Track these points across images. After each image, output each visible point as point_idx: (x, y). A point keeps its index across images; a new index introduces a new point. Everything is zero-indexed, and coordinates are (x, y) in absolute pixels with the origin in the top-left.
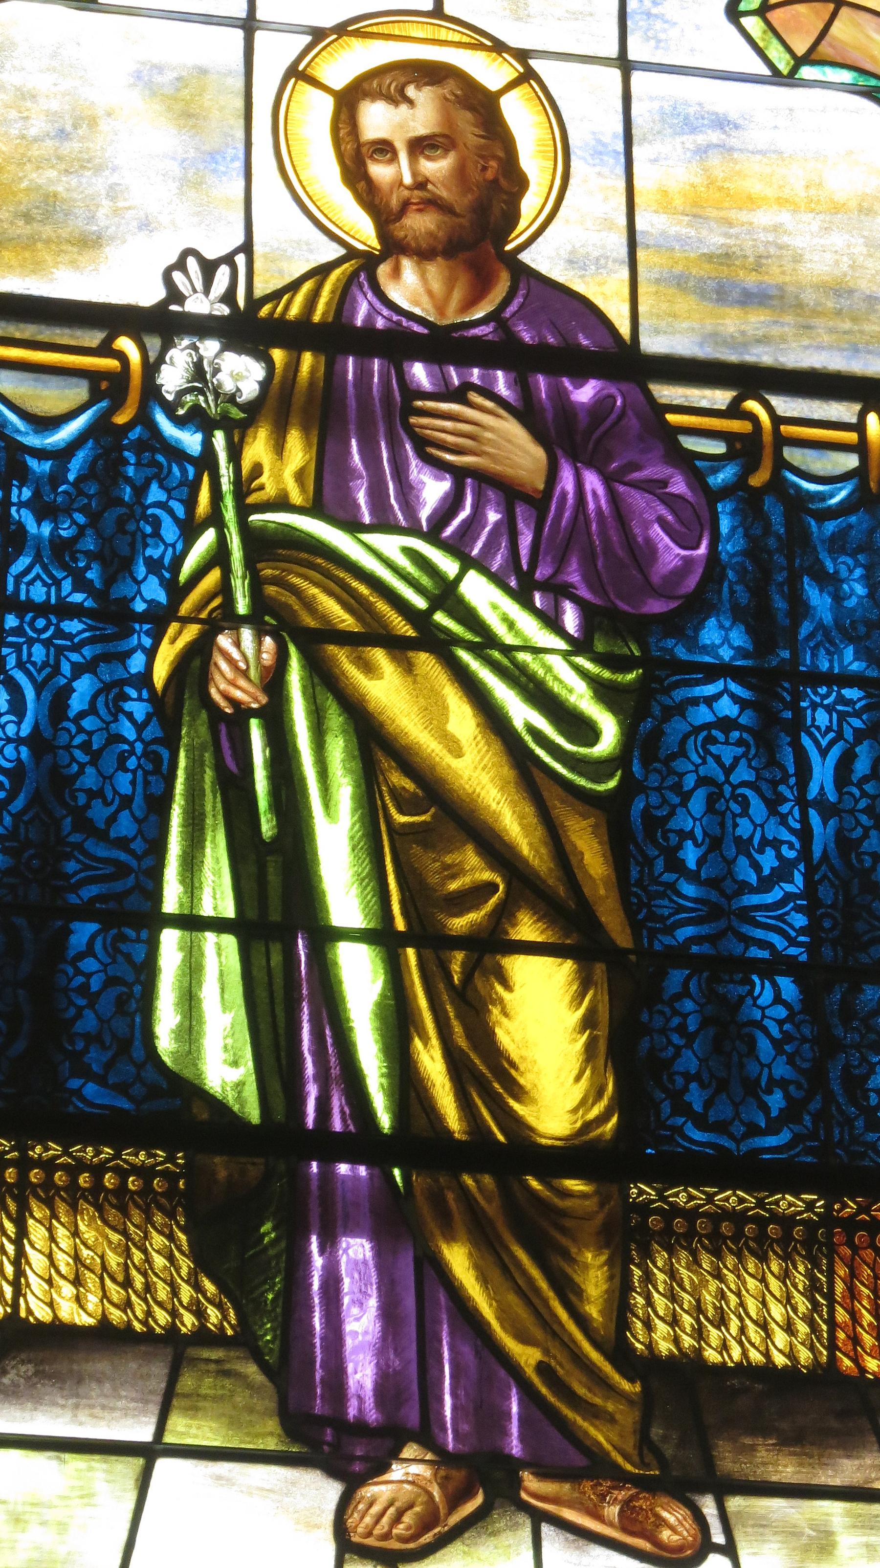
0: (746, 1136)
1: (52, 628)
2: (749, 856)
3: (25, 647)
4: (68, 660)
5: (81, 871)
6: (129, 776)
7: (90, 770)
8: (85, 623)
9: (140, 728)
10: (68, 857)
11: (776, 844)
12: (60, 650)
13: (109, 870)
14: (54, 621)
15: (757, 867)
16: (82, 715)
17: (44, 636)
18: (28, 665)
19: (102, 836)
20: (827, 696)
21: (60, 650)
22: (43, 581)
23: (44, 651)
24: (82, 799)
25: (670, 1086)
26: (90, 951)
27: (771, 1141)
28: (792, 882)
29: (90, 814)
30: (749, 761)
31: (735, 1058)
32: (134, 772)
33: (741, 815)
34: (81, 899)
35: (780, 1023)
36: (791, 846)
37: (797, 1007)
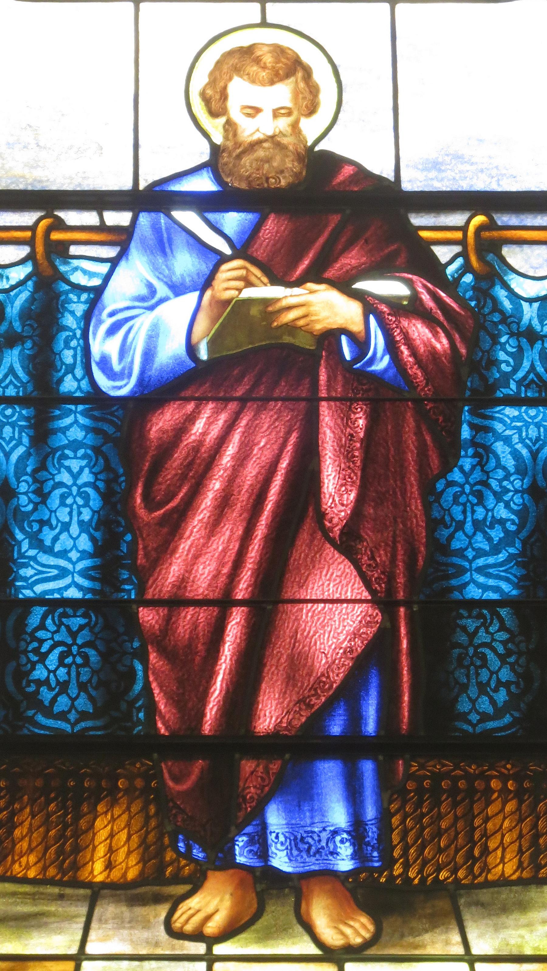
1: (17, 414)
2: (485, 533)
5: (36, 574)
6: (68, 510)
9: (75, 476)
13: (55, 572)
14: (18, 410)
15: (489, 539)
18: (527, 441)
20: (12, 415)
26: (42, 626)
28: (514, 546)
30: (91, 468)
31: (472, 669)
33: (477, 504)
35: (504, 643)
37: (512, 470)
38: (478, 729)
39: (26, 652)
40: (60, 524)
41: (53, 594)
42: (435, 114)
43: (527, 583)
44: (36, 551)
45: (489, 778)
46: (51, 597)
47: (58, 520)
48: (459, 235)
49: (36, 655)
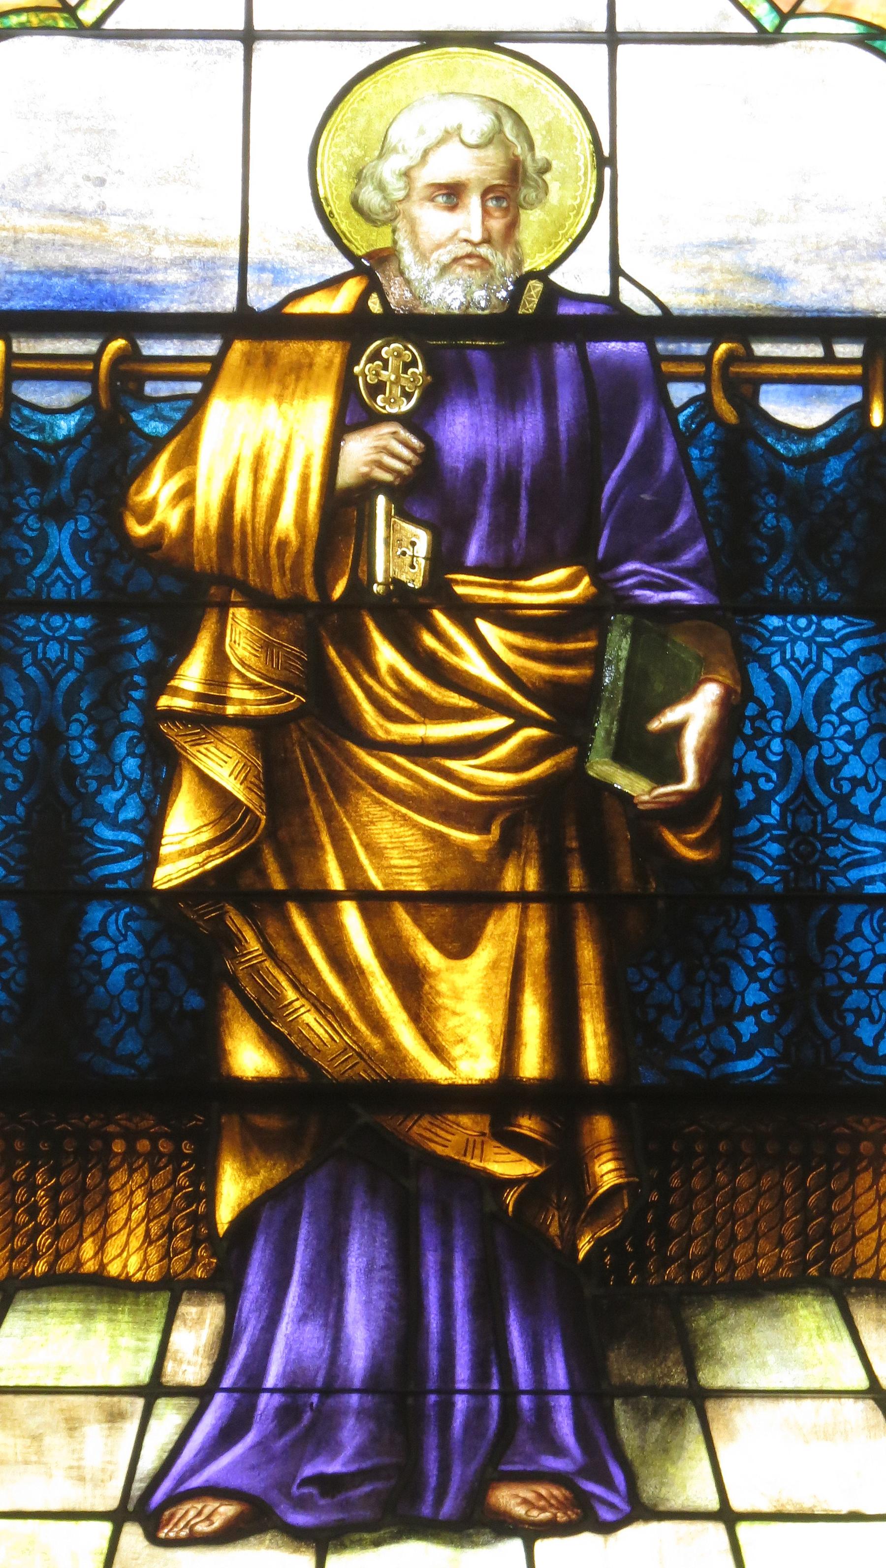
0: (715, 1063)
3: (788, 646)
4: (830, 656)
7: (853, 759)
8: (844, 620)
10: (836, 842)
11: (753, 777)
12: (822, 647)
16: (844, 707)
17: (805, 635)
18: (793, 664)
19: (868, 820)
21: (822, 647)
22: (799, 582)
23: (806, 649)
24: (846, 787)
25: (839, 1022)
27: (742, 1066)
29: (853, 801)
31: (708, 987)
32: (141, 989)
34: (849, 881)
36: (769, 779)
37: (769, 703)
38: (715, 1074)
39: (778, 966)
40: (880, 783)
41: (115, 882)
42: (776, 191)
43: (784, 867)
44: (848, 822)
45: (108, 1139)
46: (112, 886)
47: (124, 777)
48: (699, 369)
49: (849, 742)
